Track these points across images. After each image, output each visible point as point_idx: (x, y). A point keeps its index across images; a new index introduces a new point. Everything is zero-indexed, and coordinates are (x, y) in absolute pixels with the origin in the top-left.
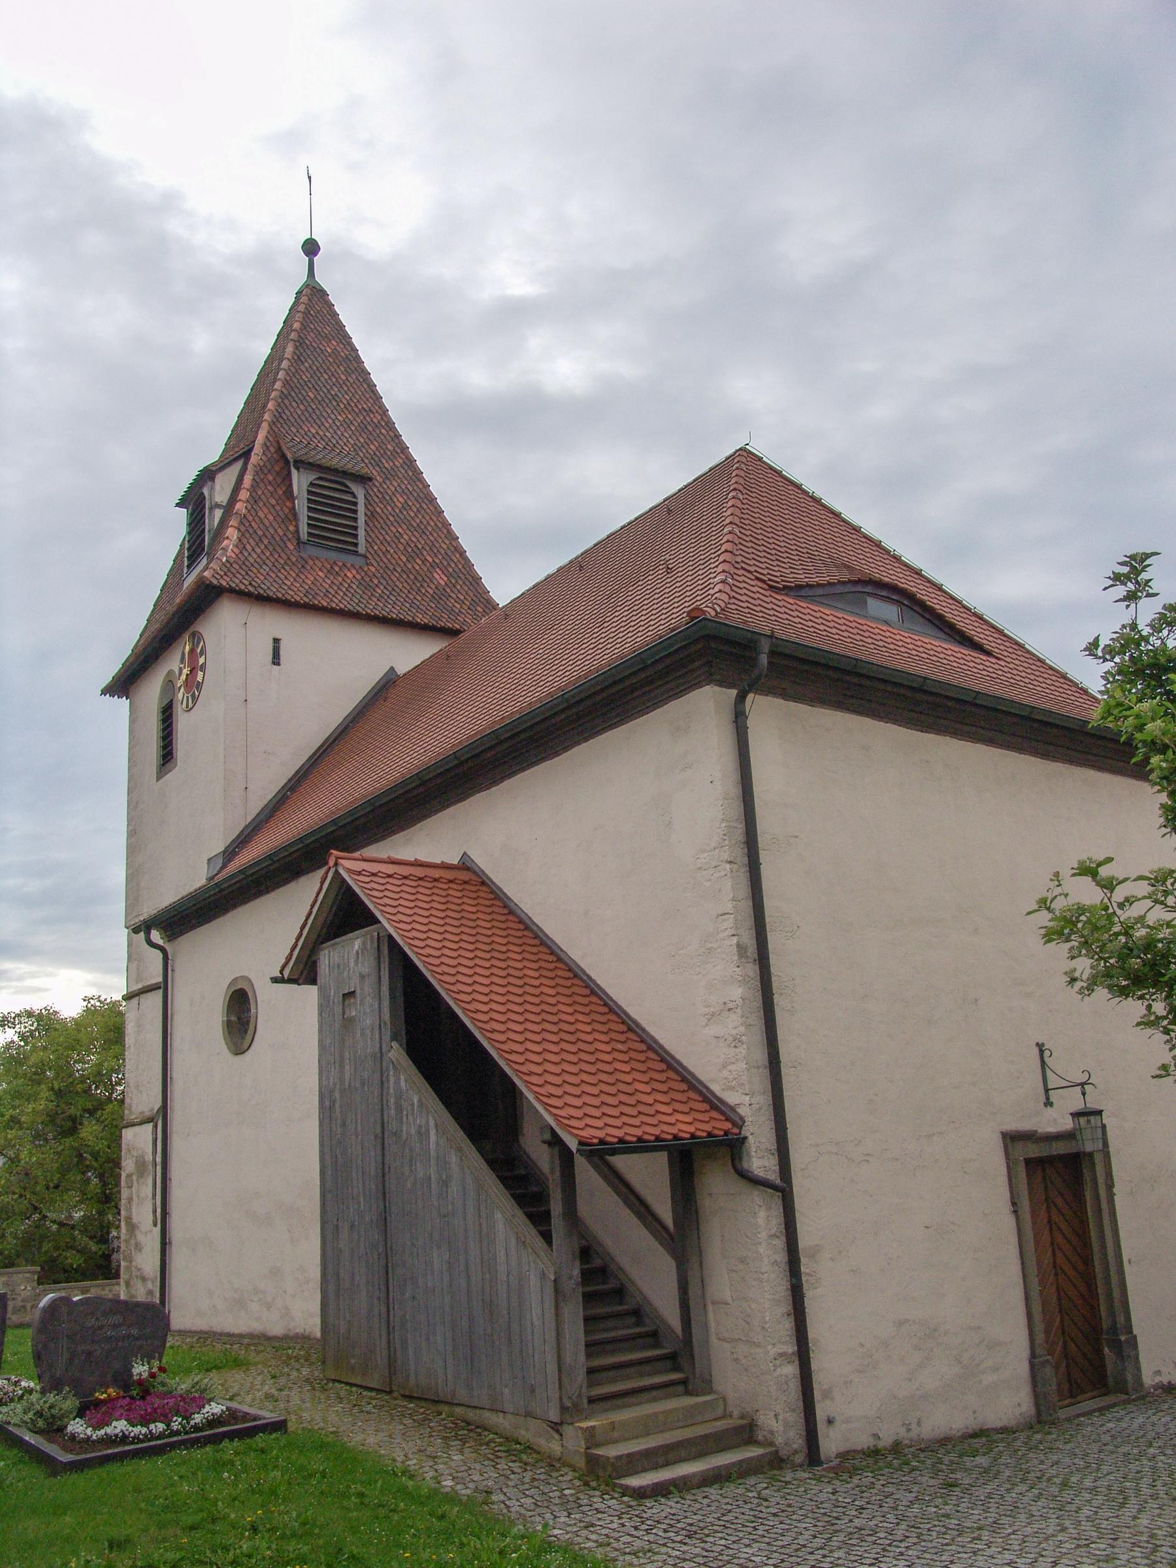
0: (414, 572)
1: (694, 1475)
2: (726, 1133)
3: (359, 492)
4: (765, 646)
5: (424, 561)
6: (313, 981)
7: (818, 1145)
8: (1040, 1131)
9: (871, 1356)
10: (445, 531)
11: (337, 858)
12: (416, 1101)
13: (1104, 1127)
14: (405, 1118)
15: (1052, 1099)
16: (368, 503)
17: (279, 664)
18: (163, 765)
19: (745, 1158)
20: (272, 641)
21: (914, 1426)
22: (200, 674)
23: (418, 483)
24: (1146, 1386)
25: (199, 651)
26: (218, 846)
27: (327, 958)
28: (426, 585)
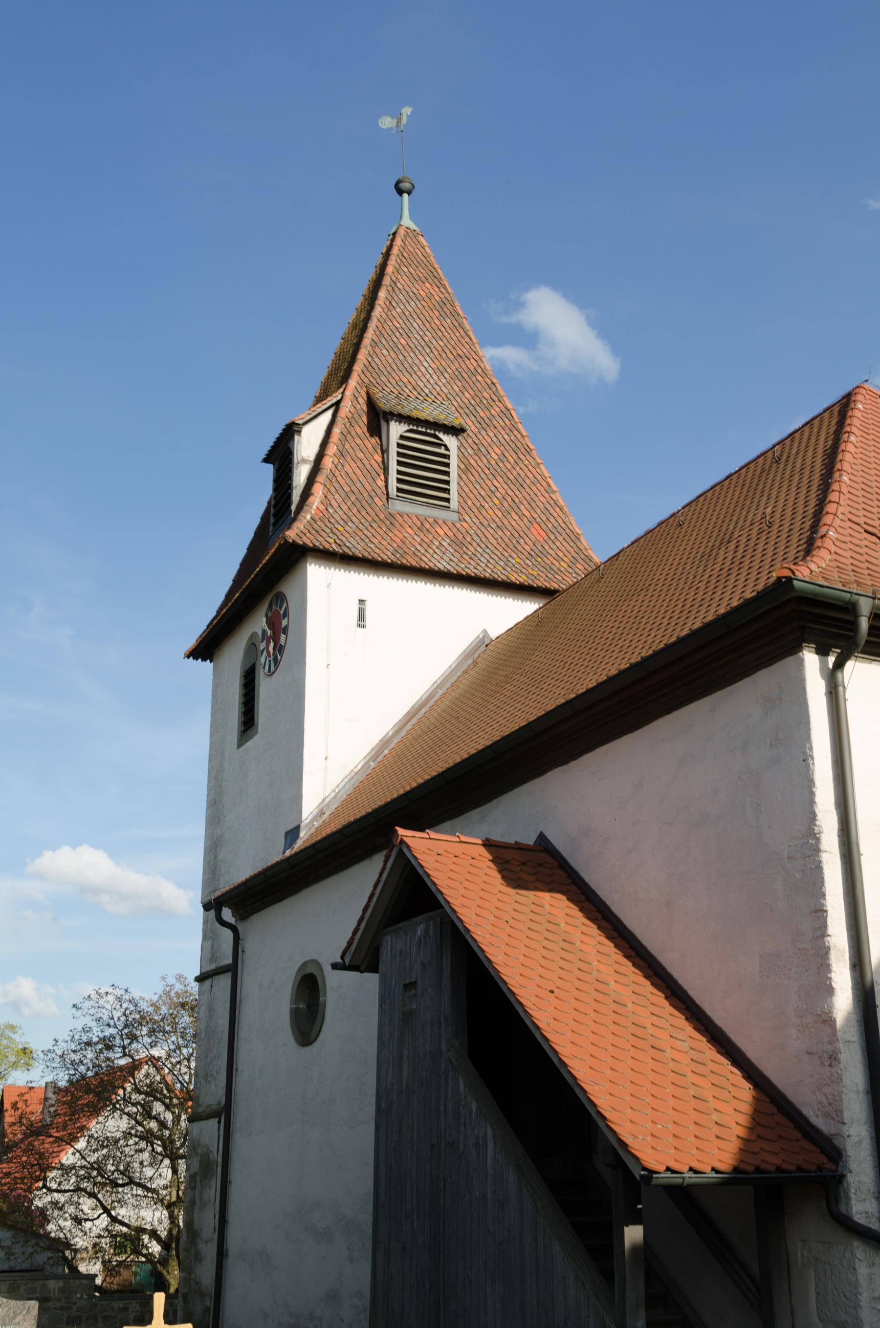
0: (510, 528)
2: (820, 1168)
3: (450, 441)
6: (375, 970)
12: (474, 1109)
16: (462, 458)
17: (364, 627)
18: (244, 731)
20: (357, 602)
22: (283, 637)
25: (282, 612)
27: (390, 945)
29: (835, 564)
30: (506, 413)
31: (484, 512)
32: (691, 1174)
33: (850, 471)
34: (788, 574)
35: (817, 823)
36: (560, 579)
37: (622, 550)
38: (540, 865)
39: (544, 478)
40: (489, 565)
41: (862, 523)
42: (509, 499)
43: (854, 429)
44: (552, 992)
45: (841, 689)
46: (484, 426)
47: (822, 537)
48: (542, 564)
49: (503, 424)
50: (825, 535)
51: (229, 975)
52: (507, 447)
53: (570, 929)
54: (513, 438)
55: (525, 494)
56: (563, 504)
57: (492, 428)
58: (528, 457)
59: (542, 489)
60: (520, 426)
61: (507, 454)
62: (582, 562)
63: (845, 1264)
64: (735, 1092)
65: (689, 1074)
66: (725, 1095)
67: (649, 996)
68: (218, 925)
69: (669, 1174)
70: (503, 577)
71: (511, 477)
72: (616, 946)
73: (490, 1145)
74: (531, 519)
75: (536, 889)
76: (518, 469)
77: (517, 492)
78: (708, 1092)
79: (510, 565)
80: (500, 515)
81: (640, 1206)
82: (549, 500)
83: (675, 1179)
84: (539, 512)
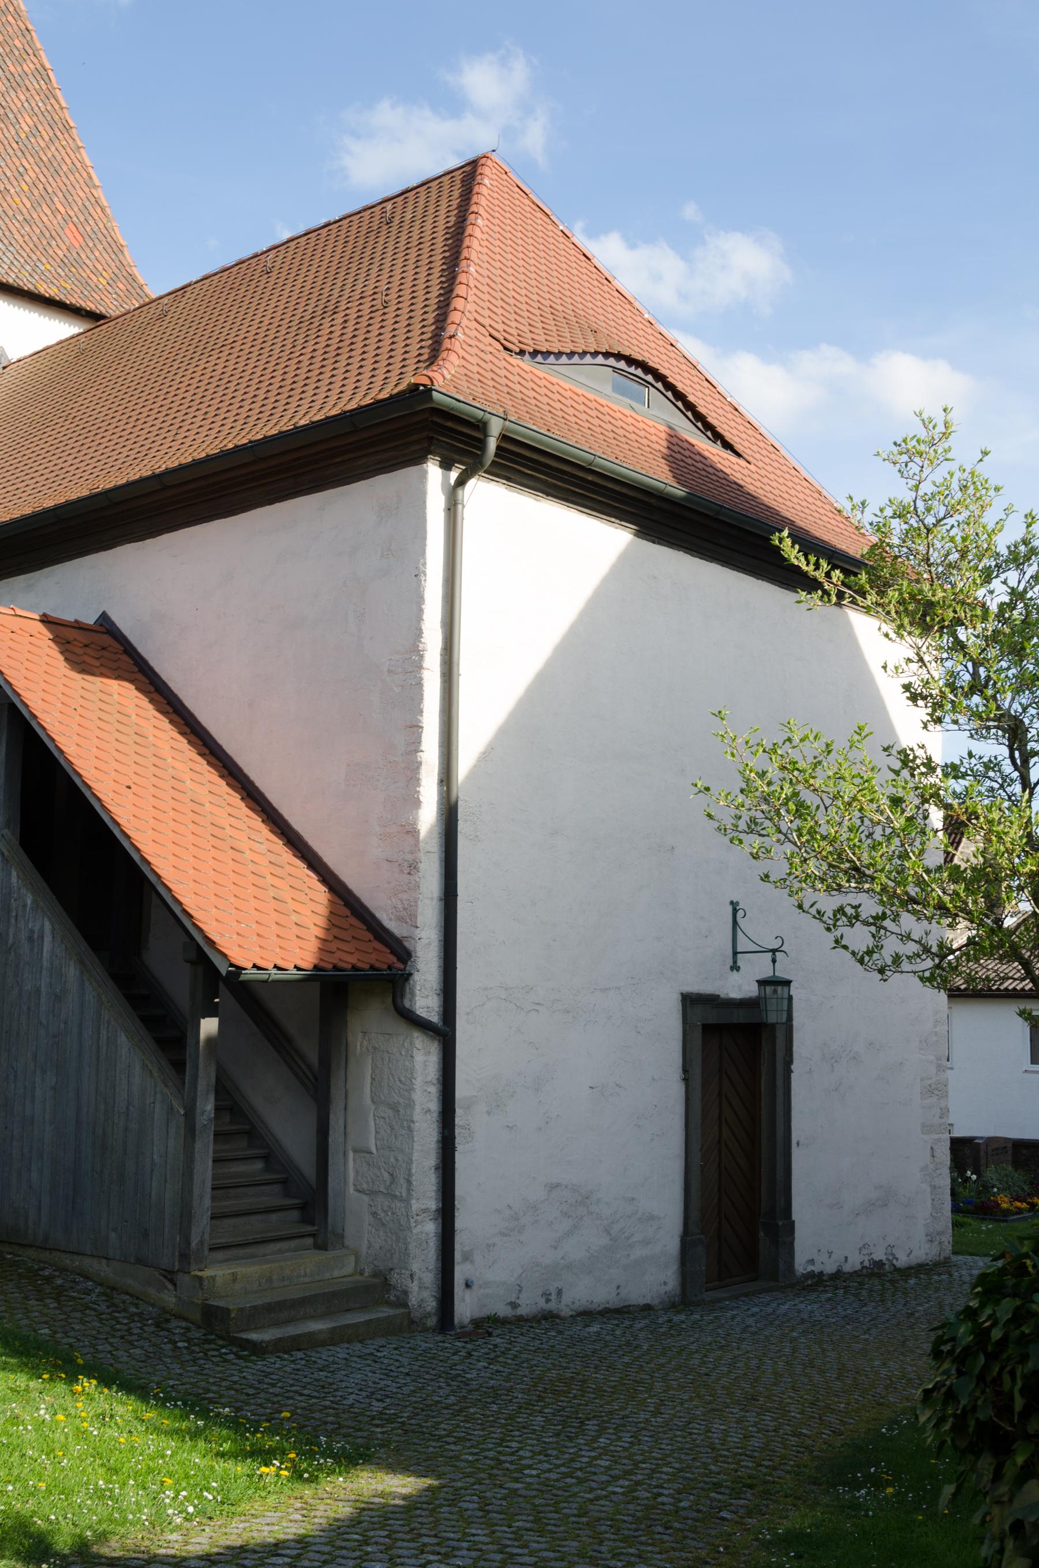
0: (40, 225)
1: (320, 1331)
2: (390, 968)
4: (495, 428)
5: (55, 212)
7: (486, 989)
8: (722, 996)
9: (518, 1220)
13: (790, 998)
14: (13, 921)
15: (739, 963)
19: (408, 996)
21: (553, 1297)
24: (798, 1274)
28: (53, 243)
29: (463, 371)
30: (42, 72)
31: (9, 199)
32: (275, 971)
33: (477, 261)
34: (427, 382)
35: (423, 640)
36: (98, 298)
37: (189, 285)
38: (104, 649)
39: (85, 167)
40: (13, 268)
41: (487, 325)
42: (41, 187)
43: (481, 211)
44: (129, 787)
45: (460, 507)
46: (14, 85)
47: (451, 337)
48: (77, 275)
49: (37, 87)
50: (453, 336)
52: (41, 117)
53: (141, 722)
54: (49, 108)
55: (60, 184)
56: (106, 204)
57: (24, 89)
58: (66, 135)
59: (81, 181)
60: (58, 93)
61: (40, 128)
62: (124, 281)
64: (312, 894)
65: (269, 876)
66: (303, 898)
67: (226, 797)
69: (255, 971)
70: (30, 286)
71: (44, 158)
72: (190, 742)
73: (48, 939)
74: (67, 218)
75: (102, 675)
76: (53, 149)
77: (51, 180)
78: (286, 894)
79: (39, 271)
80: (29, 205)
81: (217, 1000)
82: (89, 195)
83: (262, 976)
84: (76, 209)
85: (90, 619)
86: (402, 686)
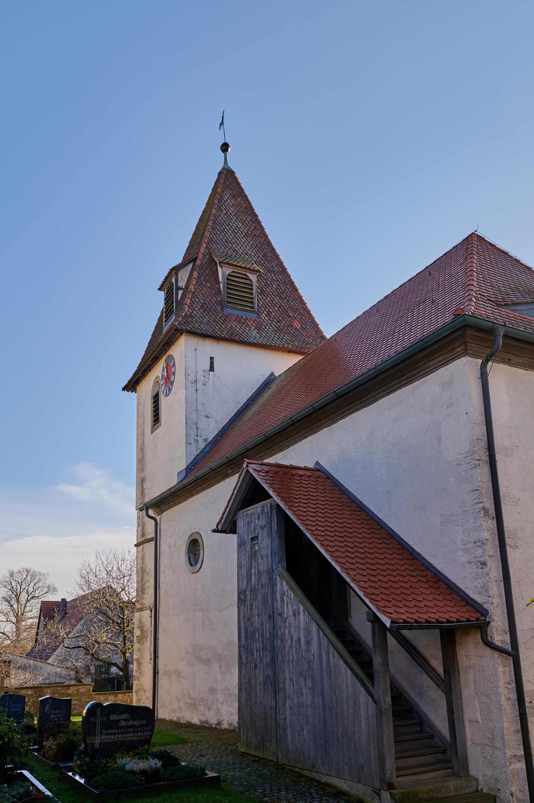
6: (235, 532)
10: (299, 300)
11: (248, 463)
18: (154, 425)
23: (285, 275)
25: (172, 365)
26: (183, 466)
38: (318, 477)
51: (153, 543)
63: (491, 666)
68: (146, 516)
73: (302, 614)
85: (311, 465)
86: (466, 471)
